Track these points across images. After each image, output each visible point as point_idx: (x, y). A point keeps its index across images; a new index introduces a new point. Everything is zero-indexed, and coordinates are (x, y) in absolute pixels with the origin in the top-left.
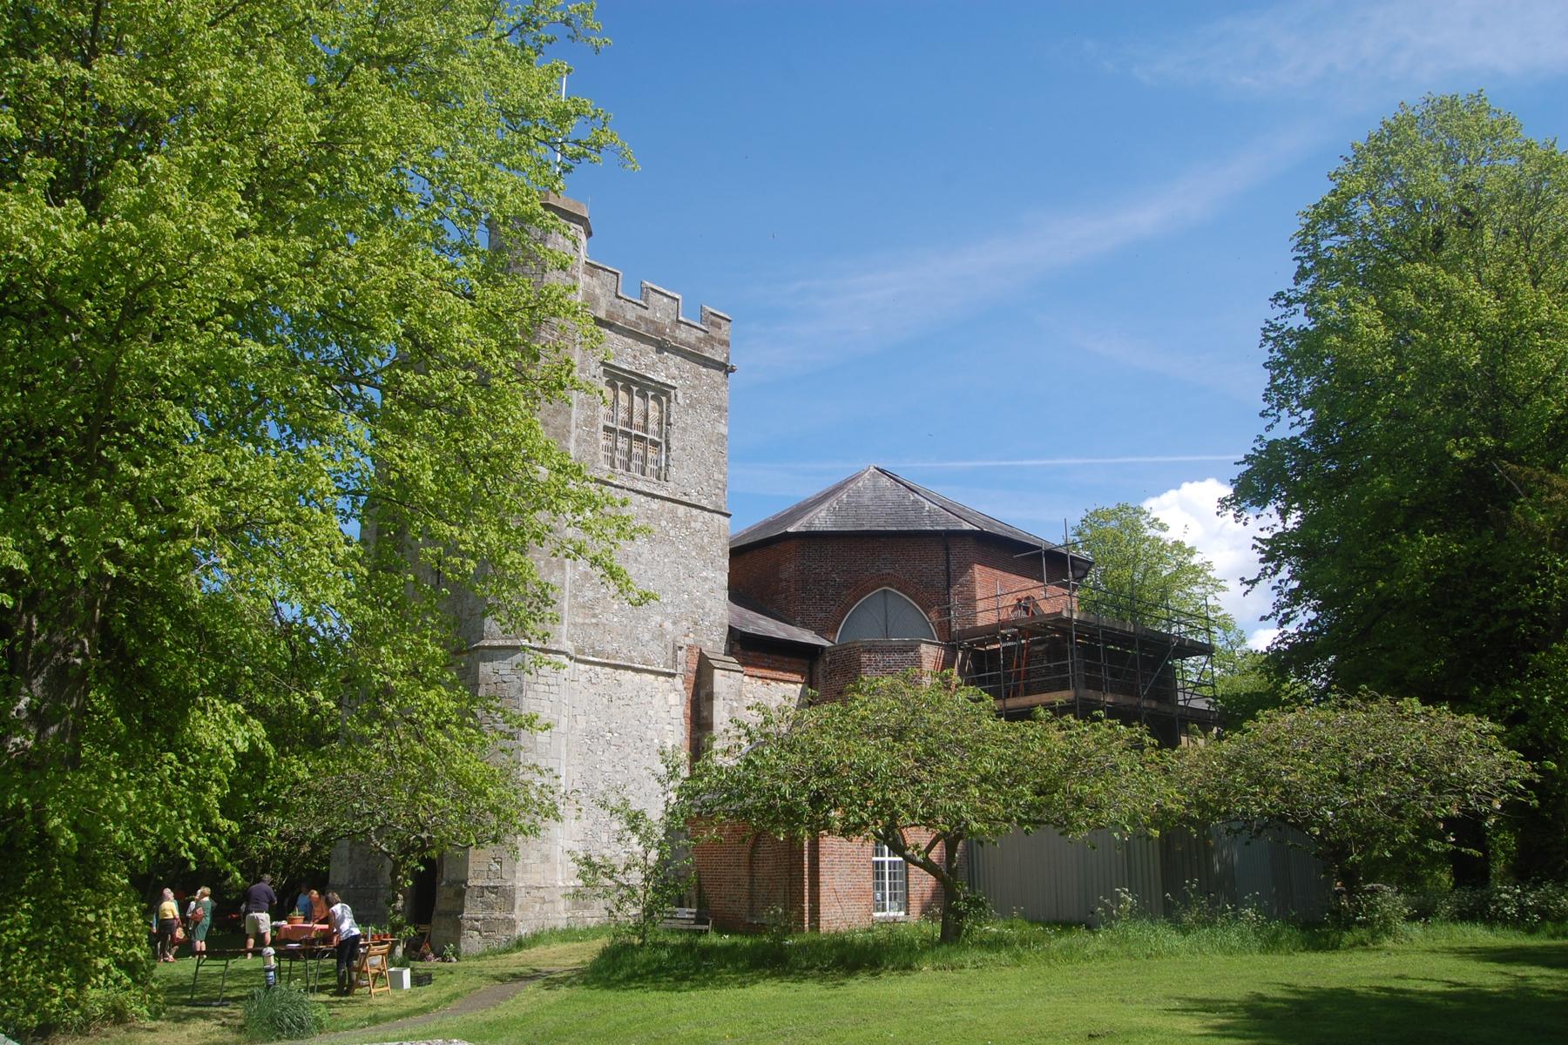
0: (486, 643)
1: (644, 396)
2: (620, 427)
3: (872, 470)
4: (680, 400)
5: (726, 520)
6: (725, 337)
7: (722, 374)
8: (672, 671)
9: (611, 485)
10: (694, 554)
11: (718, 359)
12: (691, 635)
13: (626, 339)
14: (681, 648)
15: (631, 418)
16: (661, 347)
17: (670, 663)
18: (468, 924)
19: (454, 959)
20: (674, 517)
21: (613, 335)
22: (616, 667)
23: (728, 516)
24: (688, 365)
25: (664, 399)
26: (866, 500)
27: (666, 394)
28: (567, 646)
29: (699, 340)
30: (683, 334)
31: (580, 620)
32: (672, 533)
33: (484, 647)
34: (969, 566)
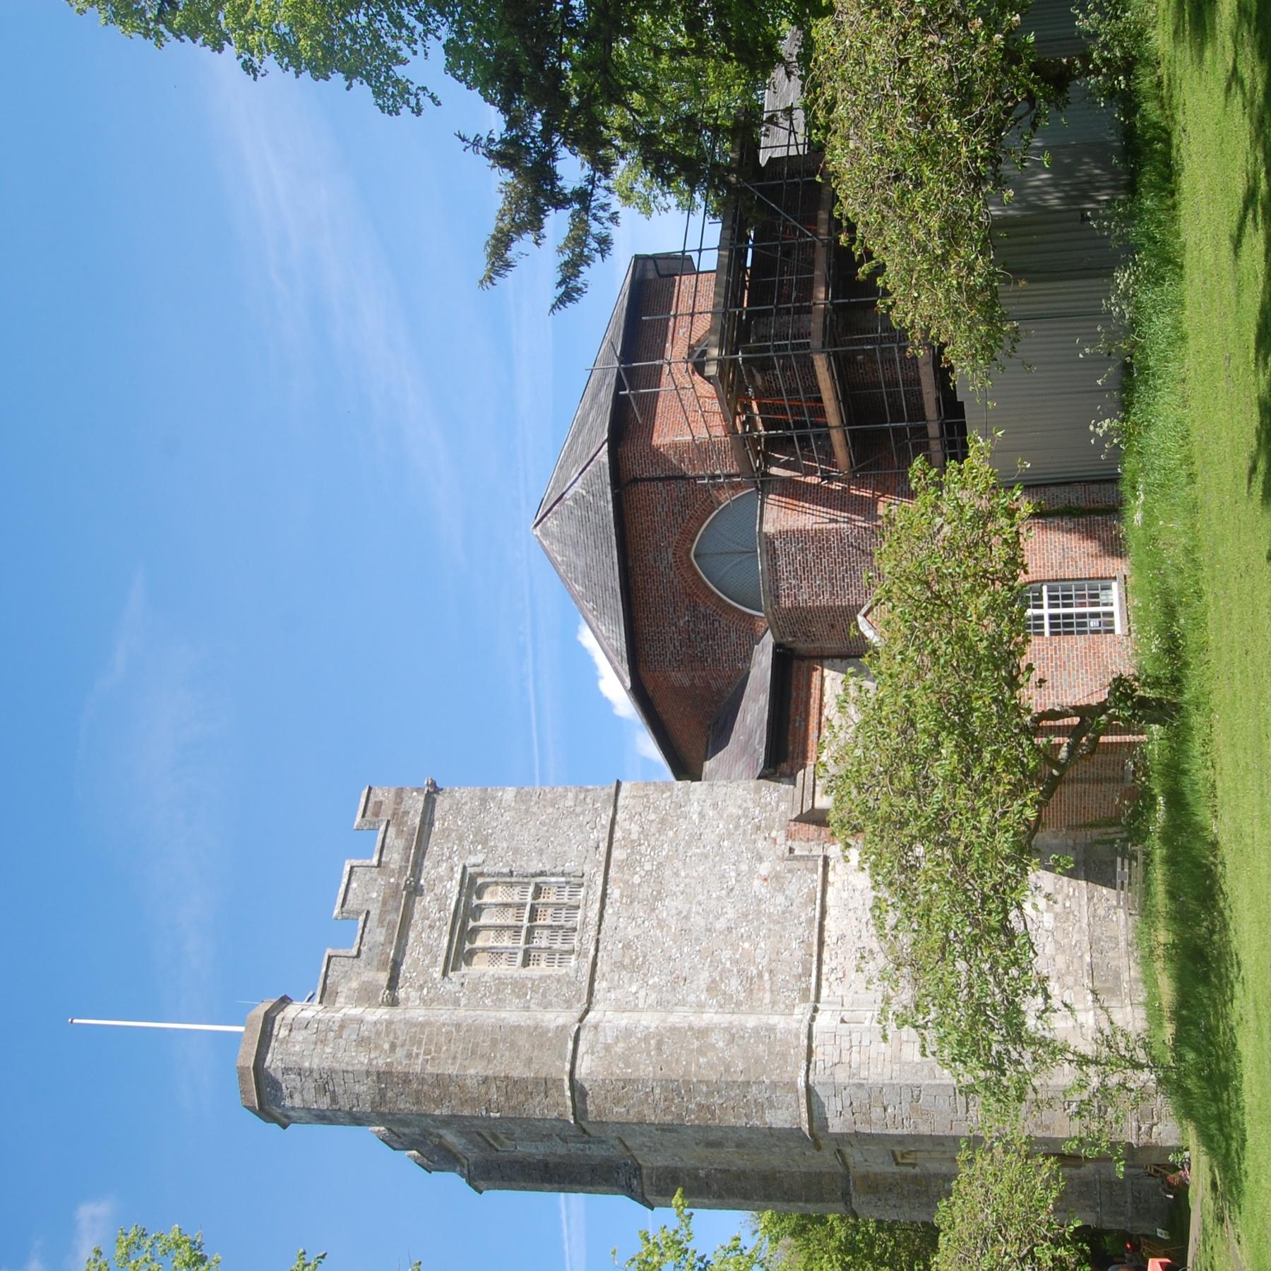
0: (805, 1127)
1: (480, 909)
3: (537, 532)
4: (479, 858)
5: (625, 786)
6: (392, 795)
7: (439, 798)
8: (820, 862)
9: (596, 957)
10: (671, 833)
11: (420, 806)
12: (774, 834)
13: (411, 941)
14: (791, 850)
15: (508, 927)
16: (415, 890)
17: (810, 865)
18: (1144, 1138)
19: (1187, 1154)
21: (407, 961)
23: (619, 784)
24: (433, 849)
25: (480, 881)
26: (580, 563)
27: (473, 879)
29: (399, 833)
30: (394, 858)
31: (767, 997)
32: (648, 867)
33: (811, 1128)
34: (655, 452)
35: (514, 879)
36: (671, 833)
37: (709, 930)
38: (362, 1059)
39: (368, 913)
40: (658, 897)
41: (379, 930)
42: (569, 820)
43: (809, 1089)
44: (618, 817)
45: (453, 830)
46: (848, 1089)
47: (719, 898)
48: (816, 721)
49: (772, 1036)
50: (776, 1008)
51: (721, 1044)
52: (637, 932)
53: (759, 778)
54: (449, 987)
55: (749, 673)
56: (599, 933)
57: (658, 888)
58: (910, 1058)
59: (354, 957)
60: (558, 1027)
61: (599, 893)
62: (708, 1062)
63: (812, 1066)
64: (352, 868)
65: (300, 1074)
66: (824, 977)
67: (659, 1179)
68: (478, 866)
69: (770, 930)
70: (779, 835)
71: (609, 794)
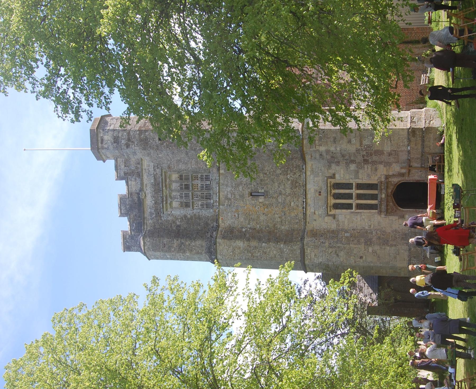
67: (225, 232)
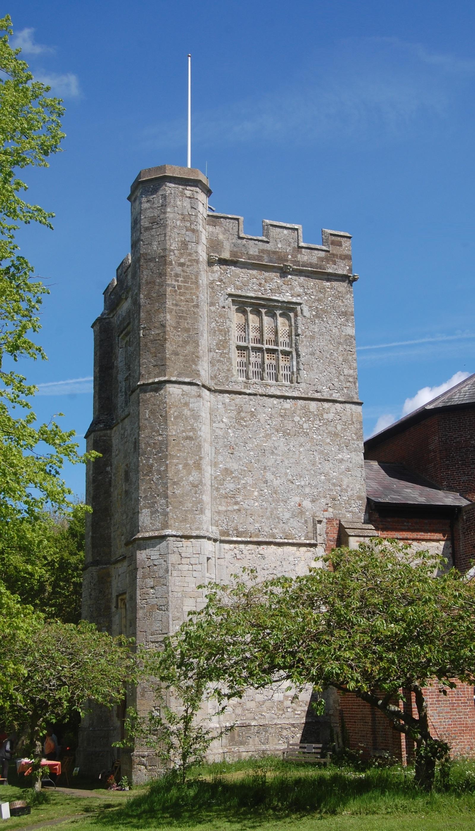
0: (140, 535)
1: (274, 316)
2: (252, 345)
4: (307, 313)
5: (359, 408)
6: (346, 252)
7: (345, 284)
8: (313, 542)
9: (245, 394)
10: (328, 440)
11: (340, 272)
12: (330, 510)
13: (251, 272)
14: (320, 522)
15: (262, 335)
16: (284, 272)
17: (311, 535)
18: (137, 760)
19: (127, 788)
20: (307, 413)
21: (237, 270)
22: (259, 543)
23: (360, 404)
24: (311, 282)
25: (292, 315)
28: (214, 531)
30: (305, 257)
31: (222, 508)
32: (305, 426)
35: (294, 337)
36: (328, 440)
37: (265, 468)
38: (174, 245)
39: (268, 242)
40: (286, 434)
41: (257, 250)
42: (334, 371)
43: (163, 538)
44: (338, 404)
45: (325, 294)
46: (165, 563)
47: (286, 474)
48: (409, 537)
49: (197, 512)
50: (216, 514)
51: (191, 479)
52: (262, 421)
53: (368, 499)
54: (222, 298)
55: (440, 490)
56: (261, 395)
57: (291, 434)
58: (186, 603)
59: (238, 235)
60: (199, 371)
61: (287, 394)
62: (179, 471)
63: (179, 539)
64: (297, 229)
65: (162, 206)
66: (236, 545)
68: (302, 313)
69: (266, 509)
70: (329, 514)
71: (353, 397)
